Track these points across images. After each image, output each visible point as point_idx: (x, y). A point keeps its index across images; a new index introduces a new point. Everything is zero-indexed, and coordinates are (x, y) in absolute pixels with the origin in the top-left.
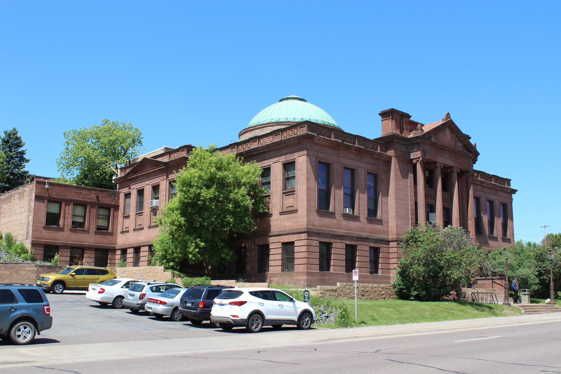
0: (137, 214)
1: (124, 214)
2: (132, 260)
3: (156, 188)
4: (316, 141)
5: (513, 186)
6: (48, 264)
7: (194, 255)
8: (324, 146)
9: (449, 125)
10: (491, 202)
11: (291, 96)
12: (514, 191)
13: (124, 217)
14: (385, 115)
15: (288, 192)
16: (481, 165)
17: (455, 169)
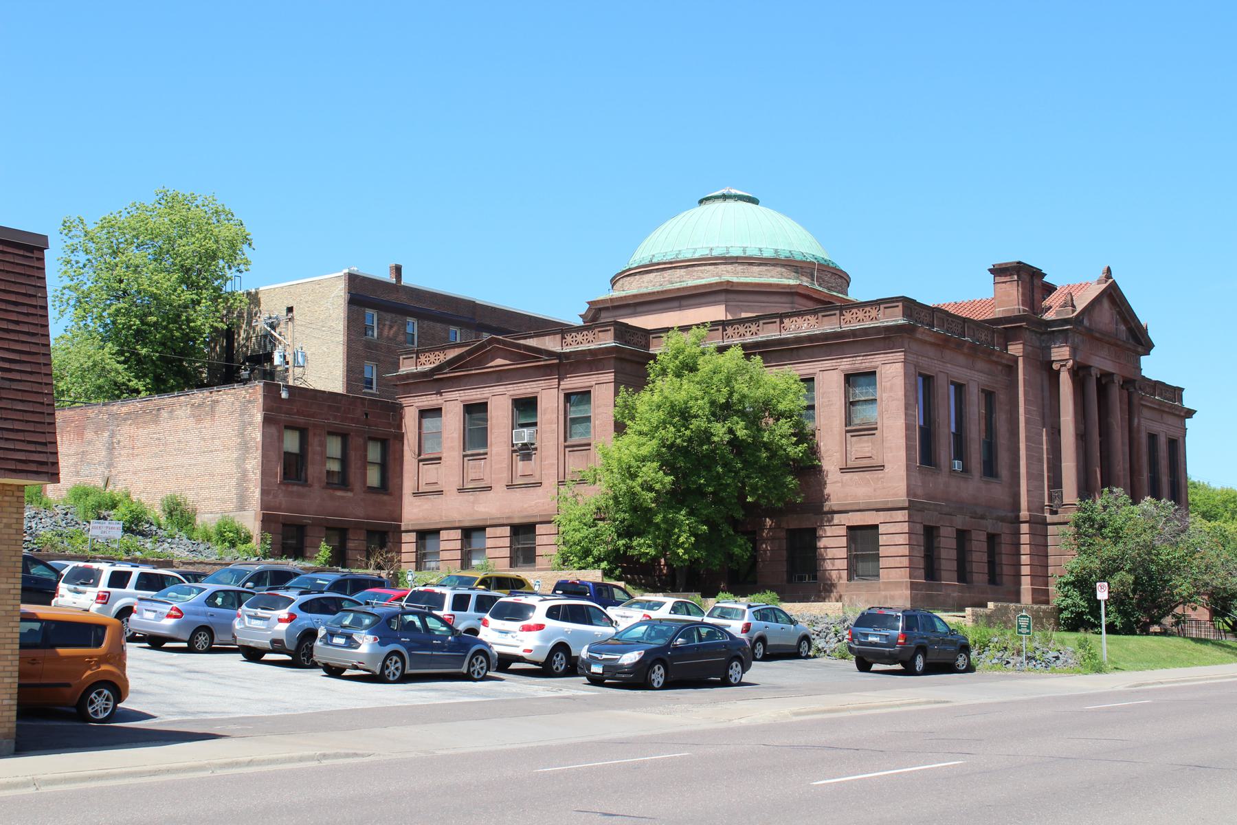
0: (464, 456)
1: (419, 455)
2: (413, 557)
3: (526, 407)
4: (919, 336)
5: (1188, 403)
6: (308, 564)
7: (686, 551)
8: (925, 342)
9: (1112, 295)
10: (960, 388)
11: (734, 191)
12: (1190, 413)
13: (420, 461)
14: (999, 271)
15: (855, 429)
16: (1152, 367)
17: (1116, 379)
